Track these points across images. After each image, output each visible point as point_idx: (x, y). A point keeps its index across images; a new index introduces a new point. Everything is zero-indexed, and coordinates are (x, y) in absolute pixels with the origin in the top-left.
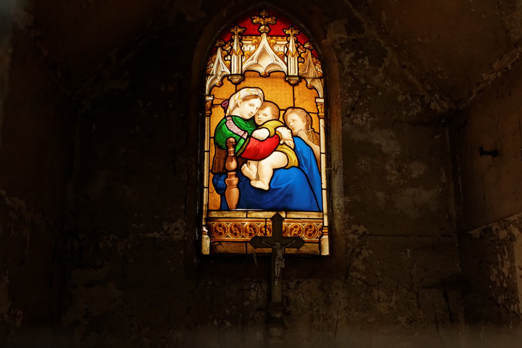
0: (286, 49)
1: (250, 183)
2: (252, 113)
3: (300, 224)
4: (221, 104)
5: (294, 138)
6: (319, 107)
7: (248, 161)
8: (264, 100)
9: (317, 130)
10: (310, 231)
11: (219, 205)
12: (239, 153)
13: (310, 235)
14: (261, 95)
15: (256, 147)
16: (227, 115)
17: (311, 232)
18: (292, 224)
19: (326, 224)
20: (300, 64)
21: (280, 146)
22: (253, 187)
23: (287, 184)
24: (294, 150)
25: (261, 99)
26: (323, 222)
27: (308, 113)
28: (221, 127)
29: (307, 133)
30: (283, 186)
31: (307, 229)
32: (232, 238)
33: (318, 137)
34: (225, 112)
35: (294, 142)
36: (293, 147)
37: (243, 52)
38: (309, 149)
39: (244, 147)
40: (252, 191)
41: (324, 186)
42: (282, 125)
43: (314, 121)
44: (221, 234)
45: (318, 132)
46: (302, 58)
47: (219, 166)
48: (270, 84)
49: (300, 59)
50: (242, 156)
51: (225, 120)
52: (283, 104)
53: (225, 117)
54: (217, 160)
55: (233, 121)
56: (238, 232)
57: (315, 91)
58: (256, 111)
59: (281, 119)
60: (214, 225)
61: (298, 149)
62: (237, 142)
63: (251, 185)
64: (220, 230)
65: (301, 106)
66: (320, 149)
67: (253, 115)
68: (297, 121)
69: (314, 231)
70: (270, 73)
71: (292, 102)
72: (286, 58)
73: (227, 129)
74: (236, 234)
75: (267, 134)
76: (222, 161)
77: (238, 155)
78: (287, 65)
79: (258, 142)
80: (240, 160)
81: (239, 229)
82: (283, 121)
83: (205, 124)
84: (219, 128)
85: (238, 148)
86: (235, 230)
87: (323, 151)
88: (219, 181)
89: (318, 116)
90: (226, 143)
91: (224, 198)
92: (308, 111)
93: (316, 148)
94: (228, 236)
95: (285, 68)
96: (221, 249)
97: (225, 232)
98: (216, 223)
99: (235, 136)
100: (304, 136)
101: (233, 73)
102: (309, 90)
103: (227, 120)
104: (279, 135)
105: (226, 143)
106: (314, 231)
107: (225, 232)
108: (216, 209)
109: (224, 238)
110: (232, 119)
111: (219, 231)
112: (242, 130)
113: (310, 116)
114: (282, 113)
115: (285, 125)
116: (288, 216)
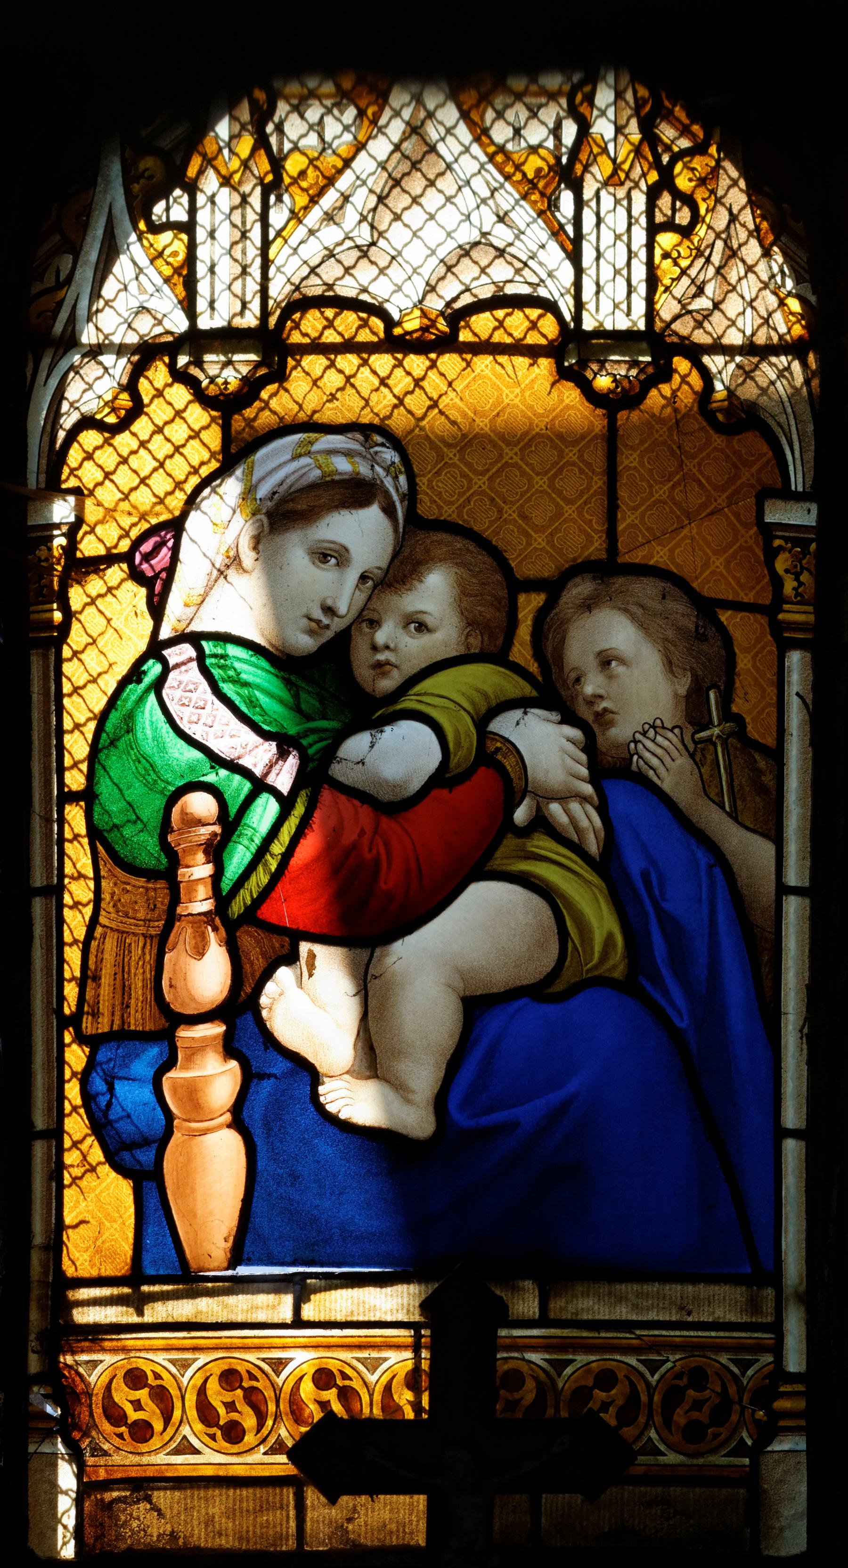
0: (570, 131)
1: (315, 1096)
2: (329, 610)
3: (632, 1361)
4: (127, 557)
5: (608, 785)
6: (781, 564)
7: (304, 947)
8: (412, 515)
9: (759, 730)
10: (697, 1405)
11: (127, 1249)
12: (245, 897)
13: (694, 1435)
14: (395, 486)
15: (354, 847)
16: (165, 633)
17: (703, 1415)
18: (581, 1359)
19: (795, 1360)
20: (666, 240)
21: (510, 843)
22: (333, 1120)
23: (555, 1097)
24: (607, 866)
25: (389, 510)
26: (778, 1350)
27: (706, 607)
28: (129, 718)
29: (698, 753)
30: (529, 1114)
31: (673, 1397)
32: (211, 1458)
33: (768, 780)
34: (157, 609)
35: (602, 810)
36: (593, 847)
37: (277, 163)
38: (703, 858)
39: (277, 848)
40: (327, 1148)
41: (792, 1115)
42: (528, 690)
43: (743, 662)
44: (142, 1432)
45: (770, 741)
46: (677, 194)
47: (124, 989)
48: (415, 582)
49: (665, 201)
50: (266, 913)
51: (153, 669)
52: (540, 540)
53: (156, 648)
54: (110, 945)
55: (205, 671)
56: (249, 1421)
57: (764, 447)
58: (361, 598)
59: (521, 651)
60: (96, 1378)
61: (635, 864)
62: (230, 823)
63: (320, 1108)
64: (137, 1405)
65: (659, 556)
66: (777, 860)
67: (337, 625)
68: (629, 662)
69: (721, 1413)
70: (457, 317)
71: (598, 525)
72: (567, 199)
73: (166, 728)
74: (233, 1433)
75: (432, 757)
76: (140, 954)
77: (237, 908)
78: (575, 256)
79: (365, 813)
80: (247, 939)
81: (254, 1399)
82: (533, 668)
83: (30, 698)
84: (112, 729)
85: (238, 857)
86: (230, 1406)
87: (795, 874)
88: (120, 1088)
89: (777, 628)
90: (166, 826)
91: (152, 1202)
92: (708, 590)
93: (750, 851)
94: (185, 1448)
95: (557, 285)
96: (146, 1524)
97: (167, 1419)
98: (108, 1359)
99: (219, 777)
100: (668, 766)
101: (205, 323)
102: (718, 440)
103: (167, 669)
104: (509, 763)
105: (166, 826)
106: (721, 1413)
107: (167, 1419)
108: (108, 1270)
109: (161, 1458)
110: (201, 658)
111: (133, 1415)
112: (266, 736)
113: (722, 630)
114: (529, 604)
115: (551, 692)
116: (309, 1312)
